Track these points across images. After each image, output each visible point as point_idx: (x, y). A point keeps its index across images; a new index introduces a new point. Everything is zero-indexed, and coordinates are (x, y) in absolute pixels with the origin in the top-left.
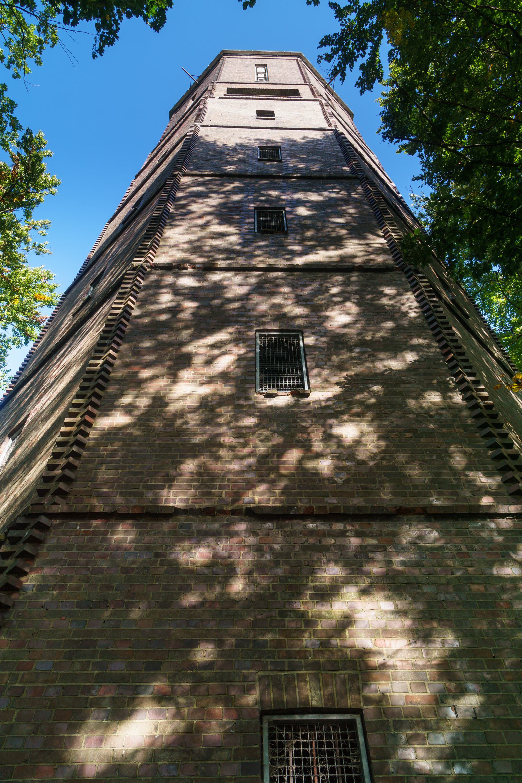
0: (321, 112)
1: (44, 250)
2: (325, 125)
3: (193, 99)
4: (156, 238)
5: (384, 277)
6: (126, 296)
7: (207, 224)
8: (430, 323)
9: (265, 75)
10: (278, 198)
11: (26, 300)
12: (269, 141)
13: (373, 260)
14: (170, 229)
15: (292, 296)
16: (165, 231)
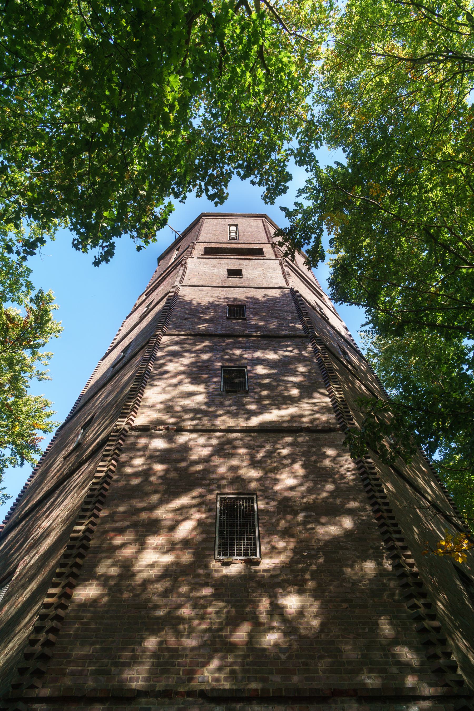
0: (281, 271)
1: (45, 376)
2: (283, 284)
3: (178, 250)
4: (137, 400)
5: (327, 437)
6: (109, 458)
7: (180, 383)
8: (366, 486)
9: (236, 234)
10: (241, 356)
11: (25, 426)
12: (235, 300)
13: (318, 419)
14: (149, 389)
15: (248, 457)
16: (145, 391)
